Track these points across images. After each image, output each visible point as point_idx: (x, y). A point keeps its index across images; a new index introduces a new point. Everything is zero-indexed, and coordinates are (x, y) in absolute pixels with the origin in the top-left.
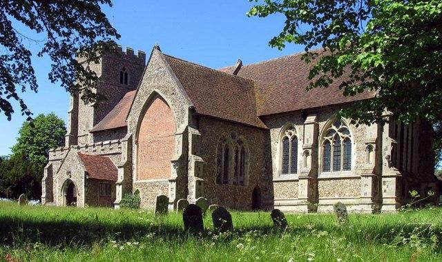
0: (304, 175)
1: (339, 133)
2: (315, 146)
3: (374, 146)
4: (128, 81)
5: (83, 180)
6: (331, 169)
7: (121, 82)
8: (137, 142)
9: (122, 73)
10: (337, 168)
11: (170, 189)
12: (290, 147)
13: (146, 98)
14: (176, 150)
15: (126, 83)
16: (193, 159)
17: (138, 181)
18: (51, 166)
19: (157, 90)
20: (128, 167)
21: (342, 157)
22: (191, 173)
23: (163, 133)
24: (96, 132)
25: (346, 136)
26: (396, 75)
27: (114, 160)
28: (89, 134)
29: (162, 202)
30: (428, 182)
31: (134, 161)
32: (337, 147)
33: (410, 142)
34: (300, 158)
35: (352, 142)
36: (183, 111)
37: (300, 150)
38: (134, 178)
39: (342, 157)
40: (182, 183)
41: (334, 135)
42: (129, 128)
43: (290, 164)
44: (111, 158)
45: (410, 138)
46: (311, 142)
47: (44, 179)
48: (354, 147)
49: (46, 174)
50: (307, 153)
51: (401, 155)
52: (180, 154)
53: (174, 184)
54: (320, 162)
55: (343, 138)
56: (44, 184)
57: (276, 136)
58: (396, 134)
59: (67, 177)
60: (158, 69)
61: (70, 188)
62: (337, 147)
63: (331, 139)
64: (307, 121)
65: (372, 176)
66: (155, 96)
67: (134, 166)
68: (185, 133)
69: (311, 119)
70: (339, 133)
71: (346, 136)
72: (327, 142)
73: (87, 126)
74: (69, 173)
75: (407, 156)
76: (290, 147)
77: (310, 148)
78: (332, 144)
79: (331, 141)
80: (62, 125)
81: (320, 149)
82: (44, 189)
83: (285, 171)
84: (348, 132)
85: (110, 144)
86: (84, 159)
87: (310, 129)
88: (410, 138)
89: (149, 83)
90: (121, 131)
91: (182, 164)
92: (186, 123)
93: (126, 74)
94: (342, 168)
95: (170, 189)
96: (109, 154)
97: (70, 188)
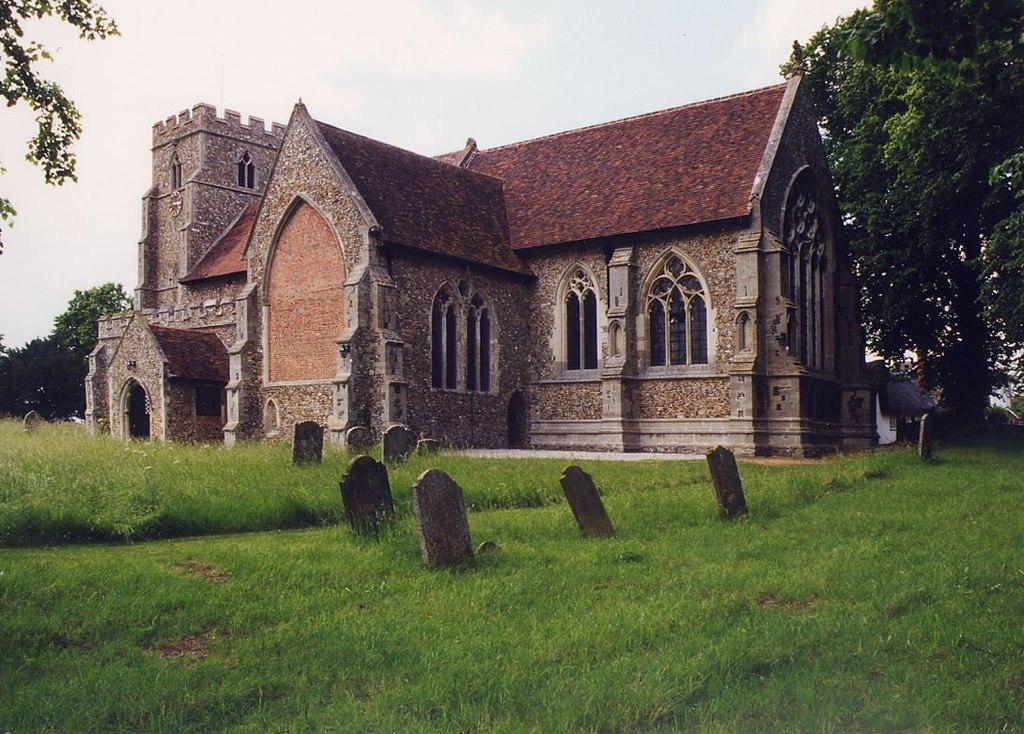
0: (611, 372)
1: (679, 286)
2: (632, 312)
3: (753, 314)
4: (256, 181)
5: (161, 381)
6: (668, 361)
7: (242, 183)
8: (267, 303)
9: (241, 166)
10: (679, 360)
11: (335, 402)
12: (581, 314)
13: (282, 211)
14: (346, 317)
15: (251, 185)
16: (382, 339)
17: (271, 384)
18: (102, 351)
19: (304, 195)
20: (251, 348)
21: (688, 337)
22: (381, 367)
23: (319, 284)
24: (192, 281)
25: (694, 293)
26: (818, 123)
27: (224, 337)
28: (180, 286)
29: (309, 436)
30: (855, 390)
31: (264, 341)
32: (678, 316)
33: (817, 307)
34: (602, 338)
35: (708, 305)
36: (358, 236)
37: (602, 320)
38: (264, 377)
39: (688, 337)
40: (361, 390)
41: (670, 291)
42: (249, 274)
43: (582, 350)
44: (220, 334)
45: (817, 299)
46: (624, 305)
47: (89, 377)
48: (711, 315)
49: (93, 368)
50: (615, 327)
51: (804, 333)
52: (354, 327)
53: (344, 392)
54: (642, 346)
55: (688, 296)
56: (89, 387)
57: (556, 289)
58: (793, 292)
59: (128, 375)
60: (304, 152)
61: (137, 399)
62: (678, 316)
63: (664, 298)
64: (614, 260)
65: (753, 376)
66: (299, 202)
67: (264, 351)
68: (366, 280)
69: (623, 256)
70: (679, 286)
71: (694, 293)
72: (656, 308)
73: (176, 272)
74: (133, 365)
75: (814, 337)
76: (581, 314)
77: (622, 317)
78: (666, 309)
79: (664, 304)
80: (884, 413)
81: (642, 321)
82: (90, 398)
83: (573, 363)
84: (698, 286)
85: (217, 307)
86: (165, 339)
87: (620, 278)
88: (817, 299)
89: (286, 184)
90: (240, 277)
91: (359, 347)
92: (364, 263)
93: (251, 167)
94: (689, 359)
95: (335, 402)
96: (214, 327)
97: (137, 399)
